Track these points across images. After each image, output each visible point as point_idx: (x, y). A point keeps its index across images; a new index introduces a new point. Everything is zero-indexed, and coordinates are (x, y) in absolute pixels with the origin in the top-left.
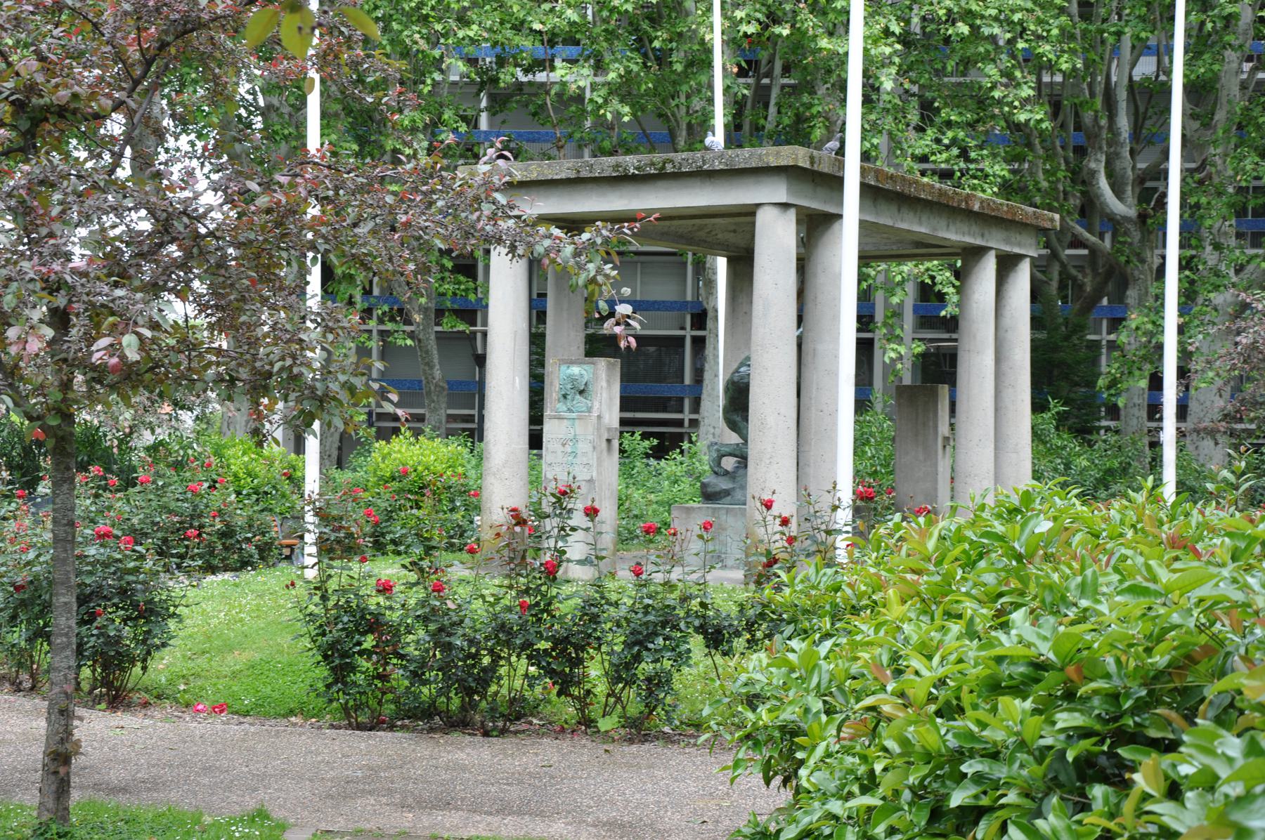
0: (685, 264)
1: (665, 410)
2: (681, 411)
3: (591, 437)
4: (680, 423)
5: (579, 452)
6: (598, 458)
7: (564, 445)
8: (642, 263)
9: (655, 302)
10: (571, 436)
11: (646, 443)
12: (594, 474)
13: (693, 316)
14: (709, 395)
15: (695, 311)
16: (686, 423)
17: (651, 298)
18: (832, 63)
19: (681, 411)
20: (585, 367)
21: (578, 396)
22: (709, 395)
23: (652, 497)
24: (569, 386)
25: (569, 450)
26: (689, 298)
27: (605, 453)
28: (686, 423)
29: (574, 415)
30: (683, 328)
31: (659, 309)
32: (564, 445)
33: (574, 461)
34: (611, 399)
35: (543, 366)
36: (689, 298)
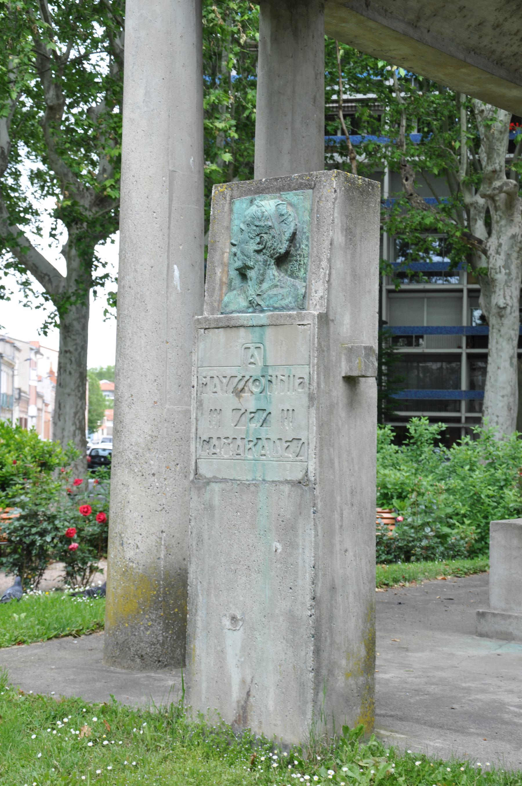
0: (461, 298)
1: (446, 410)
2: (459, 411)
3: (303, 372)
4: (458, 420)
5: (273, 409)
6: (322, 426)
7: (239, 392)
8: (428, 298)
9: (438, 328)
10: (255, 371)
11: (435, 428)
12: (312, 465)
13: (468, 338)
14: (492, 386)
15: (470, 334)
16: (463, 420)
17: (435, 324)
18: (413, 496)
19: (459, 411)
20: (291, 196)
21: (273, 271)
22: (492, 386)
23: (442, 485)
24: (253, 246)
25: (252, 406)
26: (465, 324)
27: (341, 412)
28: (463, 420)
29: (262, 318)
30: (460, 347)
31: (441, 333)
32: (239, 392)
33: (263, 433)
34: (356, 277)
35: (205, 210)
36: (465, 324)
